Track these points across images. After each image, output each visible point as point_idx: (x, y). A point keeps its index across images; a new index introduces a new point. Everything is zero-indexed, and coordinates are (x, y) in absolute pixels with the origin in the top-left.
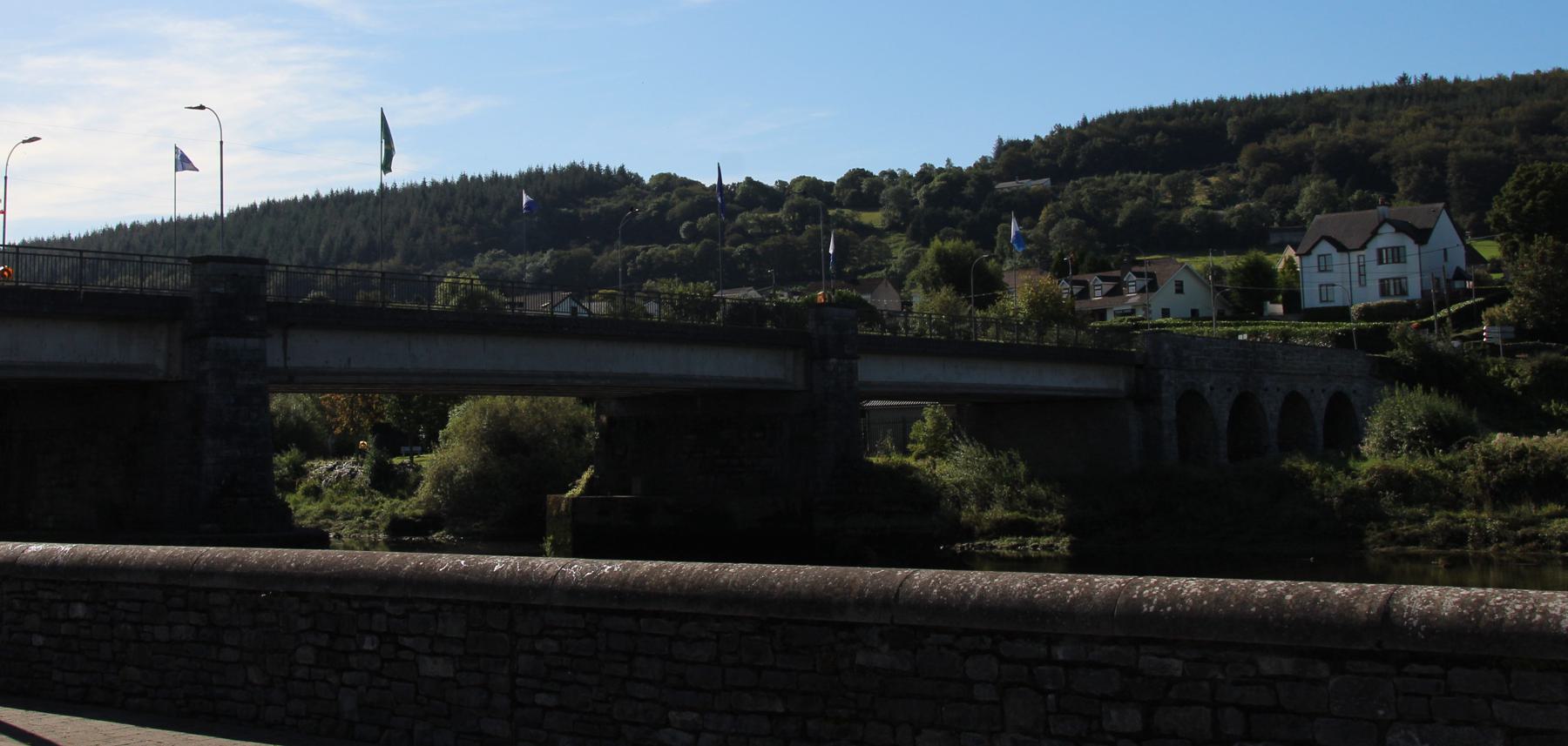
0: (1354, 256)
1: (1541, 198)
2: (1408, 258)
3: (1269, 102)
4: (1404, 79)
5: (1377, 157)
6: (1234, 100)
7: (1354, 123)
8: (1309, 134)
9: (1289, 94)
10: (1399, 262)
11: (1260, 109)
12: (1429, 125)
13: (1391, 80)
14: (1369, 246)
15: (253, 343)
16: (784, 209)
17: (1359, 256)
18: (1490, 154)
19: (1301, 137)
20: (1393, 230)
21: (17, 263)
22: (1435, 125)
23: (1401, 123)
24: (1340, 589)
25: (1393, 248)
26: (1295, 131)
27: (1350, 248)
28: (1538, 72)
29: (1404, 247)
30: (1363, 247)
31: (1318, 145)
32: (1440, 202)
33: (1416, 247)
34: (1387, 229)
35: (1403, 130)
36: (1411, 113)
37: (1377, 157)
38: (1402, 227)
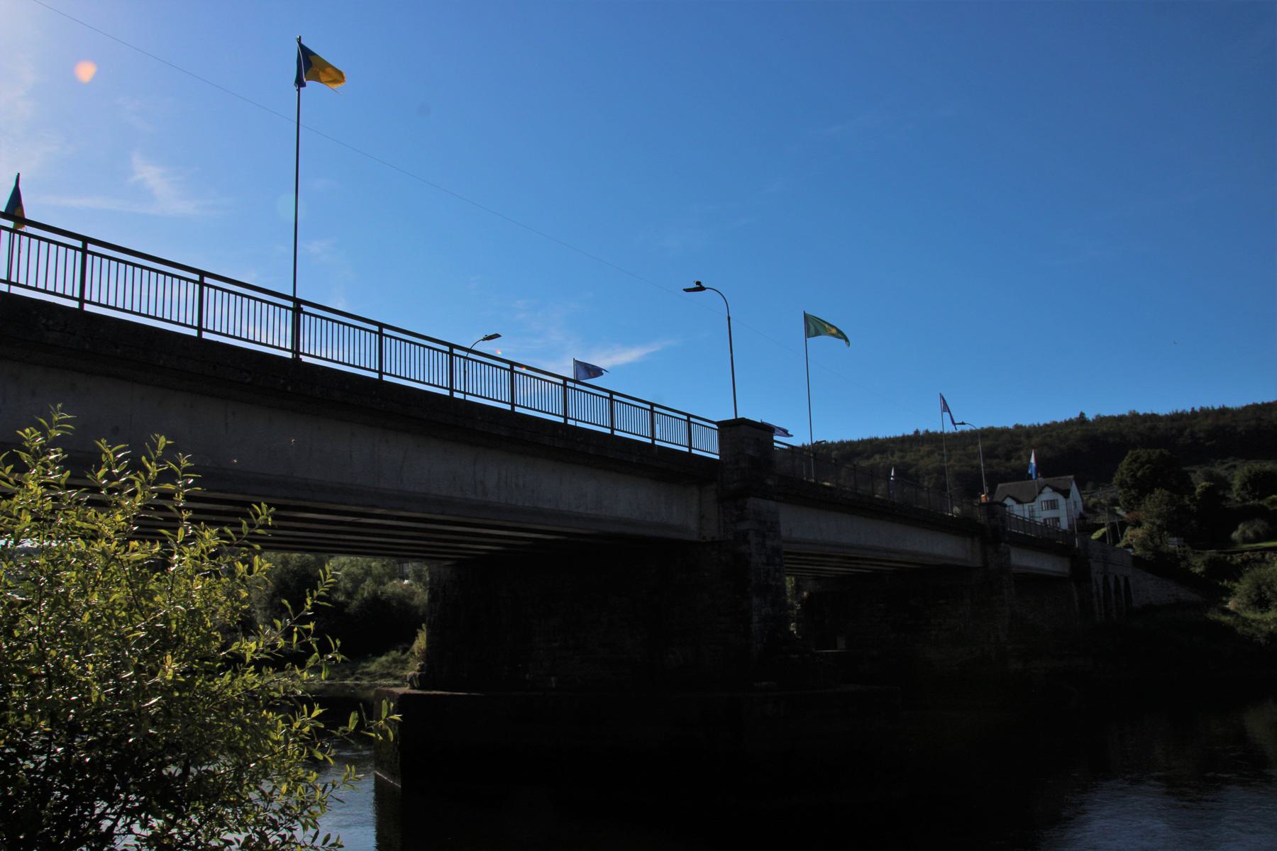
0: (1026, 506)
1: (1147, 469)
2: (1060, 507)
3: (851, 444)
4: (917, 432)
5: (912, 471)
6: (833, 443)
7: (897, 454)
8: (875, 459)
9: (860, 439)
10: (1055, 508)
11: (848, 447)
12: (936, 454)
13: (910, 432)
14: (1037, 500)
15: (772, 504)
16: (359, 597)
17: (1029, 506)
18: (969, 469)
19: (872, 461)
20: (1051, 490)
21: (857, 558)
22: (939, 454)
23: (921, 453)
24: (214, 519)
25: (1051, 501)
26: (868, 458)
27: (1024, 501)
28: (982, 428)
29: (1057, 500)
30: (1033, 501)
31: (882, 464)
32: (1070, 474)
33: (1064, 500)
34: (1047, 490)
35: (922, 458)
36: (925, 449)
37: (912, 471)
38: (1056, 490)
